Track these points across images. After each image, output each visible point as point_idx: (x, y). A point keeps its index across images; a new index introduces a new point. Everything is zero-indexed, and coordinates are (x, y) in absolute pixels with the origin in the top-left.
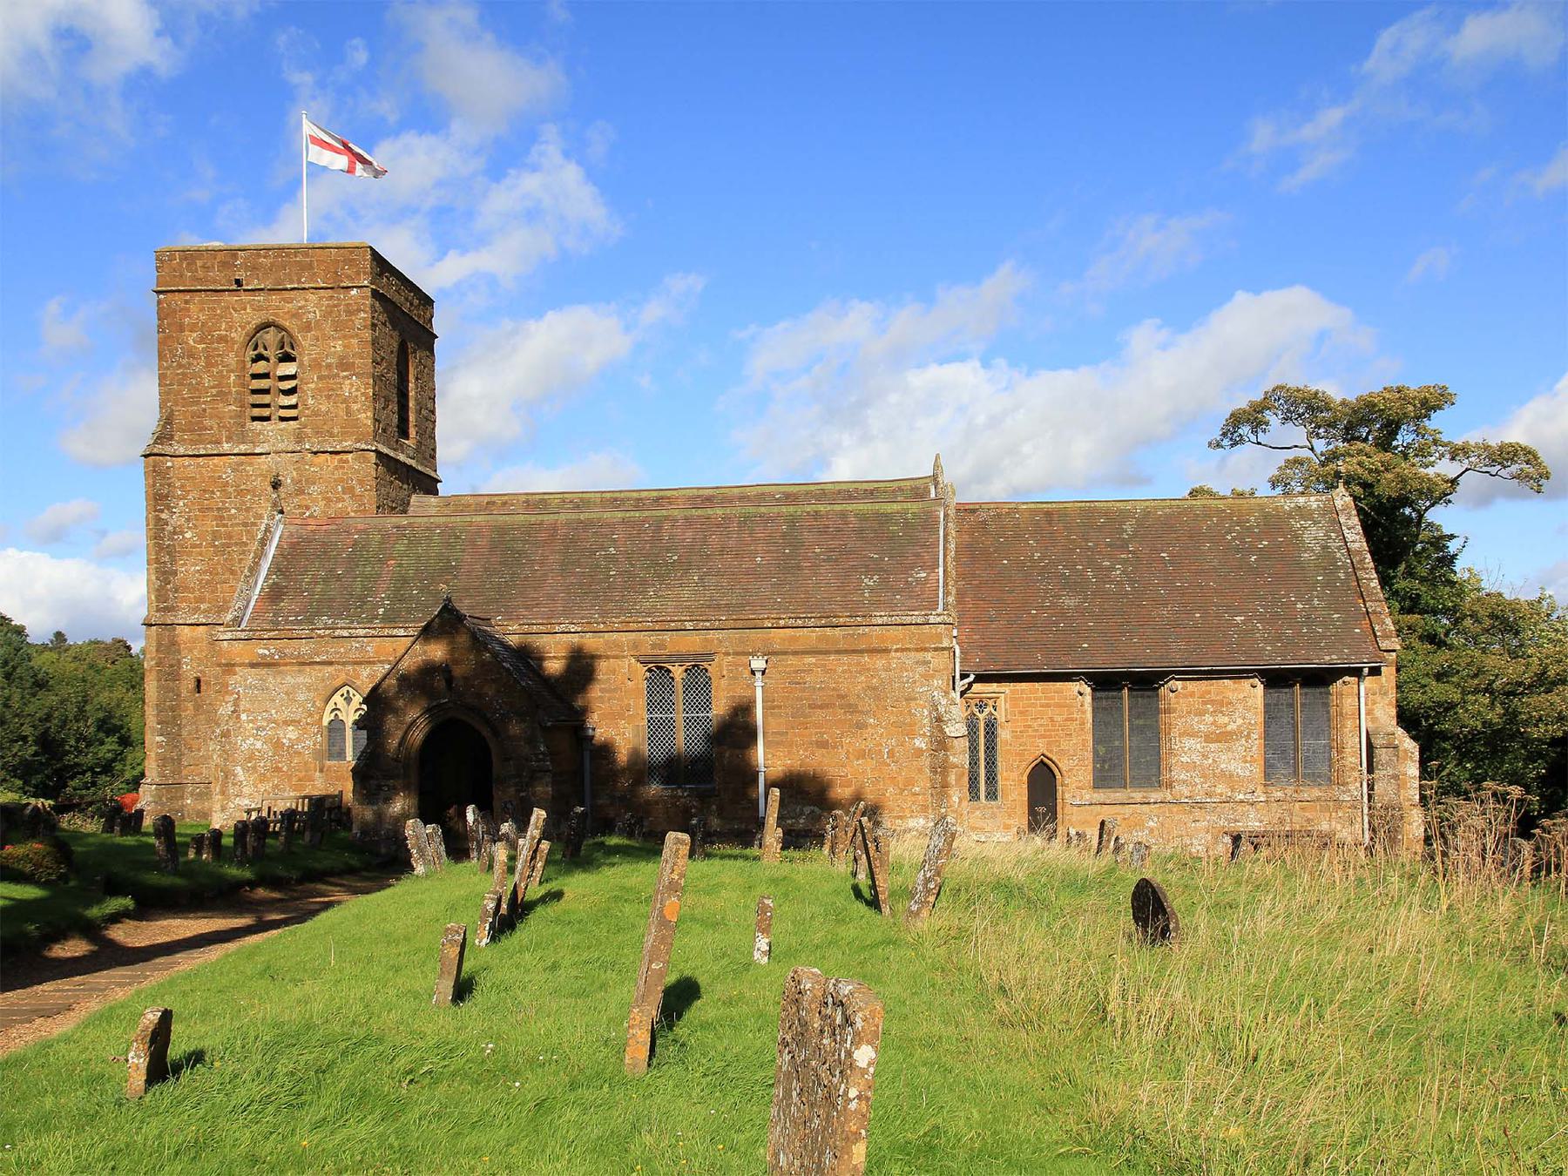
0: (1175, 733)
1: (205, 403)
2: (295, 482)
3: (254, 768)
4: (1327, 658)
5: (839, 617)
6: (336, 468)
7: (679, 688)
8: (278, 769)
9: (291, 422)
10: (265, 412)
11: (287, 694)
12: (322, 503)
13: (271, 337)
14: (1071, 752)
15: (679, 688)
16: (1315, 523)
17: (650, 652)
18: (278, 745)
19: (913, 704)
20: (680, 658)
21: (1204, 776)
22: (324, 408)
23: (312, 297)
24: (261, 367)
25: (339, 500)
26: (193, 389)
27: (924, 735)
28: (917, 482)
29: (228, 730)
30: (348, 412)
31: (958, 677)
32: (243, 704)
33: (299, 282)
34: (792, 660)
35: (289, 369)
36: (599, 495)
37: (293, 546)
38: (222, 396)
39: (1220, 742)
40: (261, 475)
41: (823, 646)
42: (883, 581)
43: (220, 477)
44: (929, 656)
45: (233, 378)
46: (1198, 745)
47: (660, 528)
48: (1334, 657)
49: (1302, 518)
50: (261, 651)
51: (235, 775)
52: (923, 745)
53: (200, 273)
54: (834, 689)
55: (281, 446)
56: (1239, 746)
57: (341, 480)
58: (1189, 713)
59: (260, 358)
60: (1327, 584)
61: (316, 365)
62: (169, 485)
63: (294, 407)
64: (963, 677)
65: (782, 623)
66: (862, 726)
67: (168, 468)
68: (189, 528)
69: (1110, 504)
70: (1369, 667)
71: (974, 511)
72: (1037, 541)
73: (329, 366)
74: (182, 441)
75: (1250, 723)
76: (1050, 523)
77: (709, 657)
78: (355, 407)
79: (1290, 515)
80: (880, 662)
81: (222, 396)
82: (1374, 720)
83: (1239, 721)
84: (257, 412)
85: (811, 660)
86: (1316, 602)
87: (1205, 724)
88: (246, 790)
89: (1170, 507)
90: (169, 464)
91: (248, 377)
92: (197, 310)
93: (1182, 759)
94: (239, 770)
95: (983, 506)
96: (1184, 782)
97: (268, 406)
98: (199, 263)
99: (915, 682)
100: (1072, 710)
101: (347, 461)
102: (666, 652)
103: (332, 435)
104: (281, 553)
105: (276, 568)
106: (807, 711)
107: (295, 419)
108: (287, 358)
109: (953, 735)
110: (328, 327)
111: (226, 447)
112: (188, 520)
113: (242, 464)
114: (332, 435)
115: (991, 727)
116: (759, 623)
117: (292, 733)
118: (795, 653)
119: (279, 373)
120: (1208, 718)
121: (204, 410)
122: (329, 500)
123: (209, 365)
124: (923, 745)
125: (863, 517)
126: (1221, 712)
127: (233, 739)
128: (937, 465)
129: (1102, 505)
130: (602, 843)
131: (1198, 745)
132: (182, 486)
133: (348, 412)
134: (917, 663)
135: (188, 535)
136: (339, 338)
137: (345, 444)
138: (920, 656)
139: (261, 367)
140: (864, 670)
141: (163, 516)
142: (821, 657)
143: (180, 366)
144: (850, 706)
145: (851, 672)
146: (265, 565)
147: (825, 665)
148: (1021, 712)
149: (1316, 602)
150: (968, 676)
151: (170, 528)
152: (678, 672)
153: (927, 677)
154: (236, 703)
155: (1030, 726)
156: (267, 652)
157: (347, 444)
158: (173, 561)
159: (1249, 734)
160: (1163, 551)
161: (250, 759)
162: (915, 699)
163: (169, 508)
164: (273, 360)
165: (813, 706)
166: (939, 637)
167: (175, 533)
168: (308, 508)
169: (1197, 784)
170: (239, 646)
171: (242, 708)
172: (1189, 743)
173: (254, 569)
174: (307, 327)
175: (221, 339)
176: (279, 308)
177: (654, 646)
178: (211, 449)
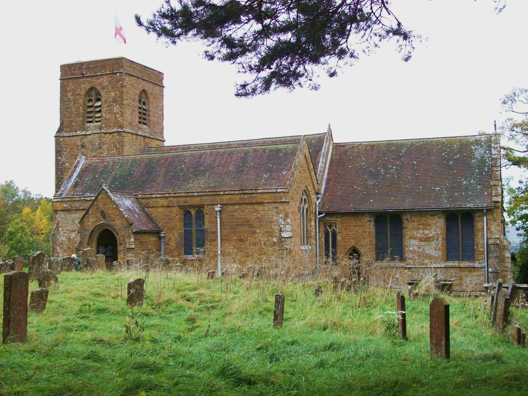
0: (407, 237)
1: (73, 117)
2: (99, 144)
3: (63, 247)
4: (469, 205)
5: (247, 190)
6: (111, 139)
7: (194, 218)
8: (69, 248)
9: (99, 123)
10: (91, 120)
11: (72, 221)
12: (107, 152)
13: (93, 93)
14: (365, 245)
15: (194, 218)
16: (481, 147)
17: (183, 204)
18: (69, 239)
19: (272, 224)
20: (194, 207)
21: (419, 256)
22: (108, 117)
23: (105, 77)
24: (90, 104)
25: (112, 150)
26: (70, 113)
27: (276, 236)
28: (321, 135)
29: (55, 234)
30: (115, 118)
31: (317, 214)
32: (60, 224)
33: (102, 72)
34: (230, 207)
35: (99, 104)
36: (208, 145)
37: (86, 167)
38: (78, 115)
39: (426, 241)
40: (89, 142)
41: (241, 202)
42: (271, 175)
43: (76, 143)
44: (278, 205)
45: (81, 108)
46: (417, 243)
47: (201, 157)
48: (472, 205)
49: (477, 145)
50: (65, 205)
51: (57, 250)
52: (276, 241)
53: (73, 72)
54: (245, 218)
55: (95, 131)
56: (433, 244)
57: (113, 143)
58: (413, 229)
59: (90, 100)
60: (480, 173)
61: (106, 101)
62: (61, 147)
63: (100, 117)
64: (320, 214)
65: (227, 192)
66: (254, 233)
67: (61, 141)
68: (67, 162)
69: (398, 141)
70: (486, 209)
71: (343, 146)
72: (365, 158)
73: (110, 101)
74: (66, 132)
75: (438, 233)
76: (372, 150)
77: (202, 206)
78: (118, 116)
79: (472, 144)
80: (261, 208)
81: (78, 115)
82: (491, 232)
83: (434, 233)
84: (89, 120)
85: (237, 207)
86: (472, 181)
87: (419, 234)
88: (60, 255)
89: (420, 142)
90: (61, 140)
91: (86, 108)
92: (71, 86)
93: (410, 249)
94: (58, 248)
95: (348, 144)
96: (411, 258)
97: (92, 117)
98: (72, 68)
99: (273, 215)
100: (365, 227)
101: (114, 136)
102: (188, 204)
103: (110, 127)
104: (83, 171)
105: (80, 176)
106: (236, 227)
107: (100, 121)
108: (98, 100)
109: (285, 236)
110: (110, 88)
111: (78, 133)
112: (67, 159)
113: (83, 138)
114: (110, 127)
115: (334, 234)
116: (219, 193)
117: (73, 235)
118: (231, 204)
119: (96, 105)
120: (421, 231)
121: (72, 120)
122: (108, 150)
123: (74, 104)
124: (276, 241)
125: (271, 151)
126: (426, 229)
127: (56, 237)
128: (329, 128)
129: (395, 142)
130: (77, 256)
131: (417, 243)
132: (65, 147)
133: (115, 118)
134: (274, 208)
135: (67, 165)
136: (113, 91)
137: (114, 129)
138: (275, 205)
139: (90, 104)
140: (256, 211)
141: (59, 158)
142: (240, 206)
143: (66, 105)
144: (250, 225)
145: (251, 211)
146: (75, 174)
147: (242, 209)
148: (345, 229)
149: (472, 181)
150: (322, 214)
151: (61, 162)
152: (193, 212)
153: (278, 213)
154: (58, 224)
155: (349, 235)
156: (66, 206)
157: (115, 130)
158: (62, 174)
159: (438, 238)
160: (415, 161)
161: (61, 244)
162: (273, 222)
163: (61, 155)
164: (94, 101)
165: (237, 225)
166: (281, 197)
167: (63, 164)
168: (102, 153)
169: (416, 259)
170: (58, 204)
171: (60, 226)
172: (413, 242)
173: (70, 177)
174: (103, 88)
175: (79, 94)
176: (96, 82)
177: (184, 202)
178: (74, 133)
